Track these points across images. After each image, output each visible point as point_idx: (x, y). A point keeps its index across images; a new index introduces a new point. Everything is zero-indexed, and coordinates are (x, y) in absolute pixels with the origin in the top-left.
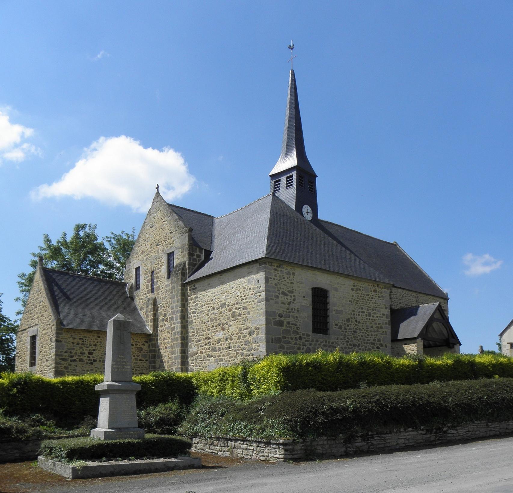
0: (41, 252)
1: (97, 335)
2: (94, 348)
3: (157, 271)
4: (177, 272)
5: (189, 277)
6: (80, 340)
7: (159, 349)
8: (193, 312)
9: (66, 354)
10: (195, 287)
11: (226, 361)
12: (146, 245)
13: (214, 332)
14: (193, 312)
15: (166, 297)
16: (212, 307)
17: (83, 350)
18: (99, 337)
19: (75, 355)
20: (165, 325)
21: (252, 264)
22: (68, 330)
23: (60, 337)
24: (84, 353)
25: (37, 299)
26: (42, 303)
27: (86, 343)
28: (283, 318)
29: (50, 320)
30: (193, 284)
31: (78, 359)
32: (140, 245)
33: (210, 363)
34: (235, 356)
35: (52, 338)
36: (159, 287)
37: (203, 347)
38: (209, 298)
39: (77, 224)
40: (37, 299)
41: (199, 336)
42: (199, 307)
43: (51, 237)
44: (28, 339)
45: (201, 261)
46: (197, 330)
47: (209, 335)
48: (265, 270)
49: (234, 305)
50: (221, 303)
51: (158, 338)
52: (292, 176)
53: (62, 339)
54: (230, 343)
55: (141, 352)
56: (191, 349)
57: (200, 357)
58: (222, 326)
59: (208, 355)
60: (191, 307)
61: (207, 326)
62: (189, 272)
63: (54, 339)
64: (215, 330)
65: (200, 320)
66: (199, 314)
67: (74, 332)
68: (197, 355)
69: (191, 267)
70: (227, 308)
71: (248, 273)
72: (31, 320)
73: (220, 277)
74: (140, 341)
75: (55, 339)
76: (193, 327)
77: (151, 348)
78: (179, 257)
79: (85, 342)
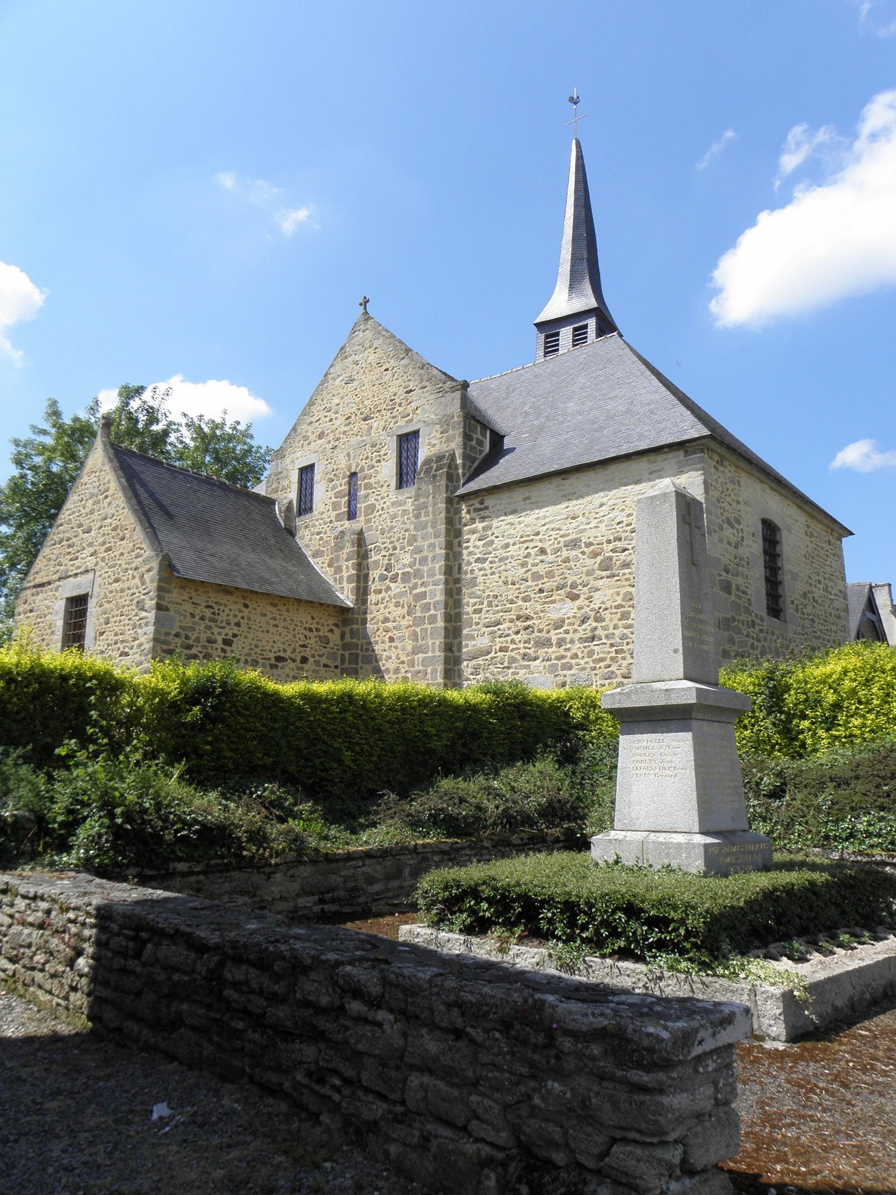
0: (33, 437)
1: (243, 601)
2: (235, 630)
3: (366, 472)
4: (433, 472)
5: (464, 484)
6: (207, 610)
7: (370, 643)
8: (478, 560)
9: (177, 640)
10: (483, 506)
11: (584, 669)
12: (331, 420)
13: (545, 603)
14: (478, 560)
15: (392, 528)
16: (537, 549)
17: (213, 633)
18: (246, 606)
19: (196, 644)
20: (388, 588)
21: (666, 452)
22: (186, 583)
23: (167, 599)
24: (215, 642)
25: (92, 512)
26: (109, 521)
27: (220, 618)
28: (730, 576)
29: (136, 558)
30: (480, 499)
31: (201, 652)
32: (313, 419)
33: (531, 673)
34: (612, 659)
35: (143, 600)
36: (372, 508)
37: (509, 639)
38: (529, 529)
39: (124, 384)
40: (92, 512)
41: (498, 612)
42: (495, 549)
43: (61, 407)
44: (60, 606)
45: (484, 453)
46: (491, 599)
47: (529, 610)
48: (701, 465)
49: (609, 542)
50: (566, 539)
51: (366, 619)
52: (586, 327)
53: (169, 603)
54: (596, 629)
55: (325, 647)
56: (471, 643)
57: (498, 659)
58: (568, 589)
59: (525, 655)
60: (471, 549)
61: (522, 590)
62: (464, 475)
63: (150, 603)
64: (548, 600)
65: (500, 577)
66: (498, 564)
67: (197, 590)
68: (490, 655)
69: (468, 464)
70: (585, 549)
71: (651, 473)
72: (71, 560)
73: (563, 481)
74: (325, 623)
75: (154, 602)
76: (478, 593)
77: (348, 639)
78: (435, 442)
79: (219, 614)
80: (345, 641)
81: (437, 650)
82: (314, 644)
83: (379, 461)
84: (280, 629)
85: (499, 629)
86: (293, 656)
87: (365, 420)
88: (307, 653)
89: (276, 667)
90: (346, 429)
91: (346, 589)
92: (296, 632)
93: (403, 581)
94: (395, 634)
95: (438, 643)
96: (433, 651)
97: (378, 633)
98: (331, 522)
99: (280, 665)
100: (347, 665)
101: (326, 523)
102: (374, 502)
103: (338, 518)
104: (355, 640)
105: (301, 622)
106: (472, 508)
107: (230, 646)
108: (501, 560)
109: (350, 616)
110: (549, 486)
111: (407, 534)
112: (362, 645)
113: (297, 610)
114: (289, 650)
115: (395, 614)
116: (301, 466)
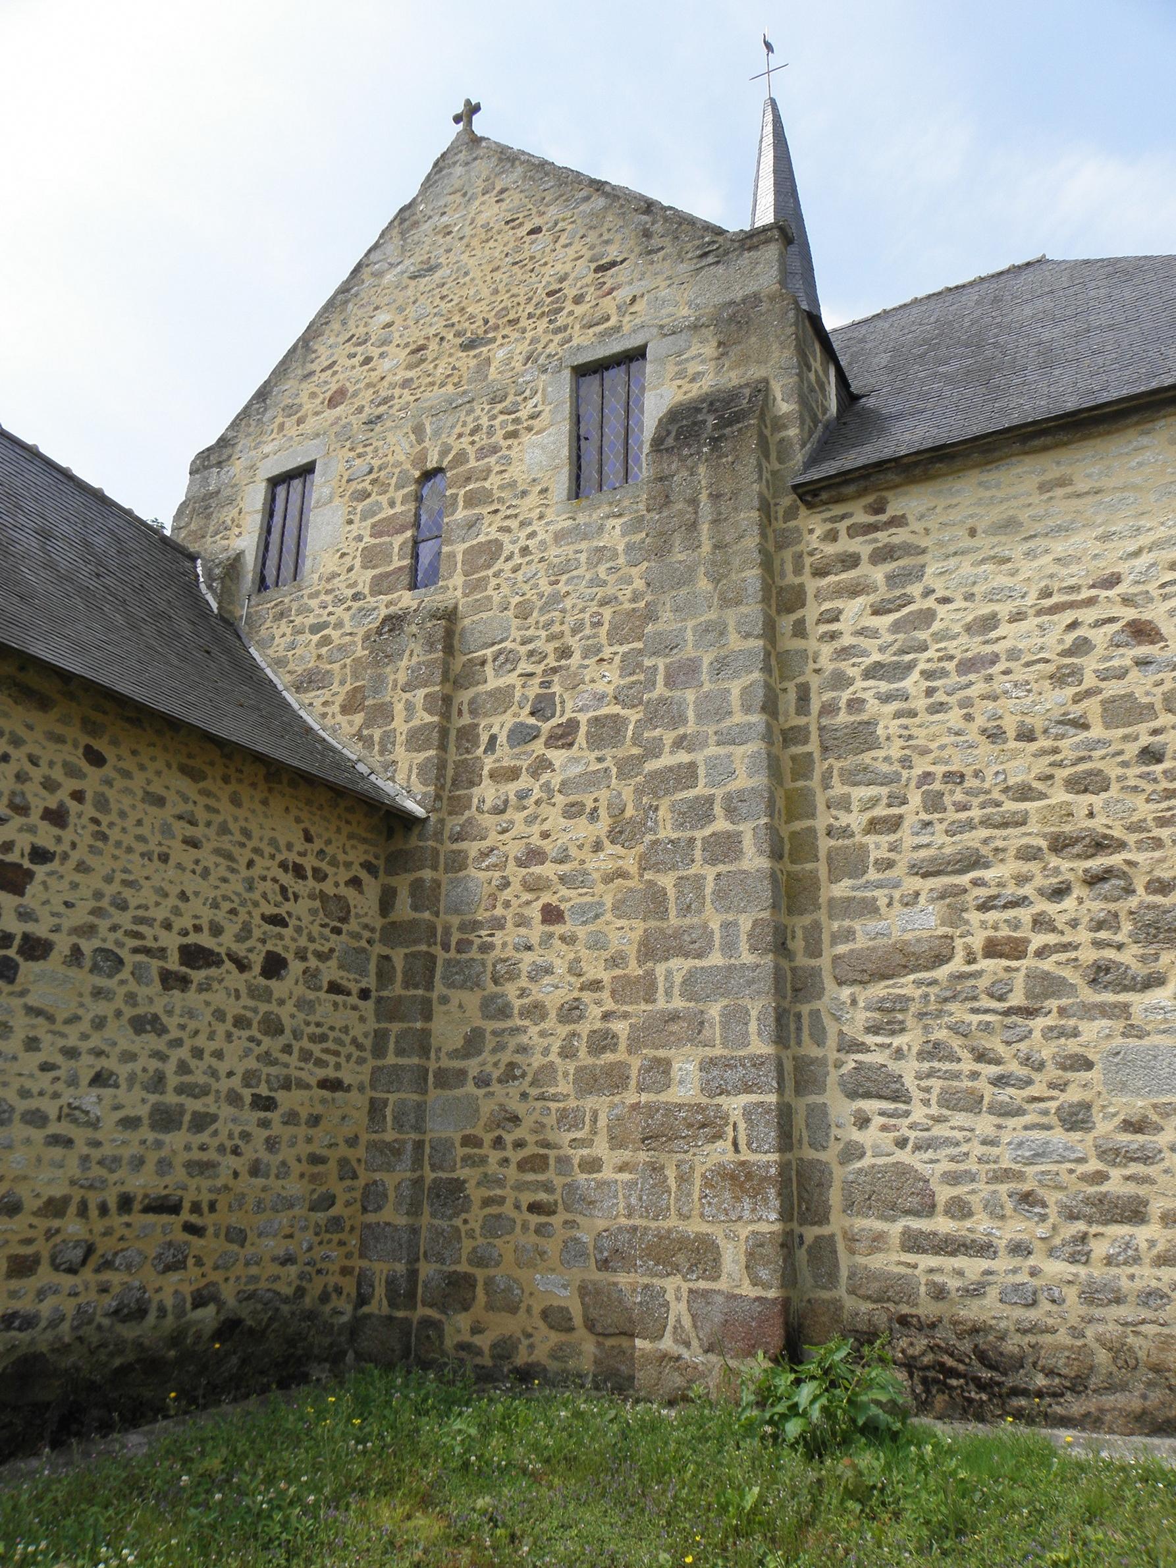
1: (85, 740)
2: (46, 836)
3: (473, 463)
8: (873, 672)
10: (883, 518)
12: (368, 360)
14: (873, 672)
15: (556, 598)
16: (1117, 626)
18: (96, 758)
20: (543, 765)
30: (870, 499)
37: (1024, 915)
41: (970, 825)
42: (939, 637)
46: (937, 786)
55: (337, 931)
60: (847, 640)
66: (954, 679)
74: (341, 857)
76: (885, 768)
78: (700, 368)
80: (393, 917)
81: (744, 945)
82: (307, 919)
83: (513, 435)
84: (208, 858)
85: (976, 883)
86: (240, 949)
87: (468, 346)
88: (285, 943)
89: (184, 982)
90: (410, 374)
91: (403, 767)
92: (256, 871)
93: (595, 742)
94: (566, 897)
95: (745, 923)
96: (729, 947)
97: (507, 894)
98: (356, 597)
99: (197, 976)
100: (397, 989)
101: (342, 601)
102: (494, 535)
103: (380, 585)
104: (427, 915)
105: (273, 842)
106: (842, 526)
107: (19, 891)
108: (967, 666)
109: (414, 842)
110: (1145, 440)
111: (607, 613)
112: (447, 931)
113: (265, 802)
114: (231, 929)
115: (564, 839)
116: (276, 472)
